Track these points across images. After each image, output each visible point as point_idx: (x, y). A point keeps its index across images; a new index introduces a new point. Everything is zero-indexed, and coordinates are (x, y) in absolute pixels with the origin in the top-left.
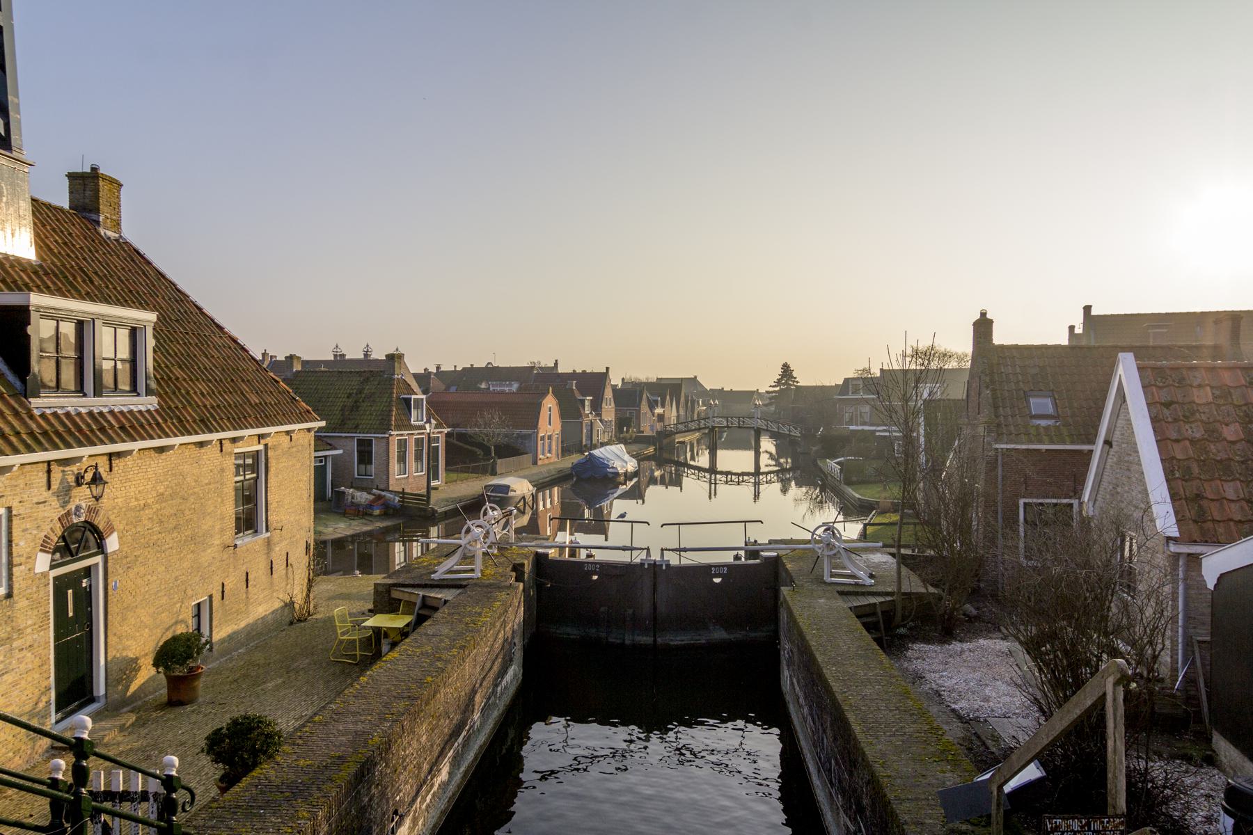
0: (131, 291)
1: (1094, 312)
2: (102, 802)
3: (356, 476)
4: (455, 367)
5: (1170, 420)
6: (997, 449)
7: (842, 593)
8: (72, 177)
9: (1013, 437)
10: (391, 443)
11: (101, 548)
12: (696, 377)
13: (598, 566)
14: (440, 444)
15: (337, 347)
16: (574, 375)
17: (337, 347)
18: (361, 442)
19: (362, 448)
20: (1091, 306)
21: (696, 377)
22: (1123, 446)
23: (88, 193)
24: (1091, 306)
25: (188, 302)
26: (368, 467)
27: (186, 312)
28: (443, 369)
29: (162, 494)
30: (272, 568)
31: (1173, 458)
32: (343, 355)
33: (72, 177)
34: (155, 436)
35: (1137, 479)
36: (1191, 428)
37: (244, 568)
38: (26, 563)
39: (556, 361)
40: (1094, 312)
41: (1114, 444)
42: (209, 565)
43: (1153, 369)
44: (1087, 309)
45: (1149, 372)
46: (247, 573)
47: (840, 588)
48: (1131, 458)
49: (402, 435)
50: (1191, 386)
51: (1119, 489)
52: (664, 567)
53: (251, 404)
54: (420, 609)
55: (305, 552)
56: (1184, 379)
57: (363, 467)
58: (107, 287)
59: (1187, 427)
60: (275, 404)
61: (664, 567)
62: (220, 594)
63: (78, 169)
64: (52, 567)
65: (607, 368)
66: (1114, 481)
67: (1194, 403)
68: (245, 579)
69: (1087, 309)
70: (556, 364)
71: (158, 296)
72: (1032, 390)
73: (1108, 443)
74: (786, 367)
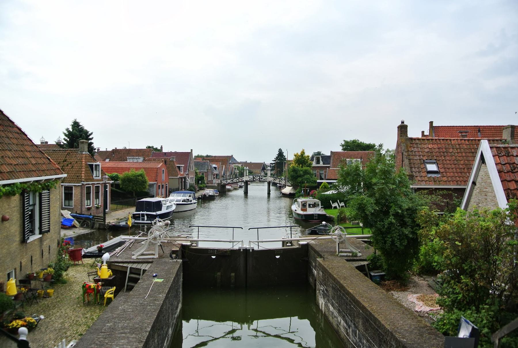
1: (434, 125)
4: (106, 149)
5: (505, 171)
7: (347, 260)
10: (83, 188)
12: (232, 156)
13: (216, 251)
15: (43, 137)
16: (171, 154)
17: (43, 137)
18: (66, 188)
19: (67, 192)
20: (433, 122)
21: (232, 156)
22: (482, 184)
24: (433, 122)
28: (101, 150)
30: (42, 254)
31: (509, 189)
32: (47, 142)
34: (20, 177)
35: (491, 200)
36: (515, 175)
37: (30, 253)
39: (162, 146)
40: (434, 125)
41: (477, 183)
42: (14, 252)
43: (497, 148)
44: (431, 123)
45: (495, 149)
46: (32, 257)
47: (346, 258)
48: (487, 190)
49: (89, 184)
50: (513, 156)
51: (480, 205)
52: (251, 251)
54: (129, 274)
55: (57, 245)
56: (509, 152)
57: (67, 202)
59: (513, 174)
61: (251, 251)
62: (20, 267)
65: (192, 150)
66: (477, 201)
67: (515, 164)
68: (30, 260)
69: (431, 123)
70: (162, 147)
72: (427, 160)
73: (474, 183)
74: (280, 150)
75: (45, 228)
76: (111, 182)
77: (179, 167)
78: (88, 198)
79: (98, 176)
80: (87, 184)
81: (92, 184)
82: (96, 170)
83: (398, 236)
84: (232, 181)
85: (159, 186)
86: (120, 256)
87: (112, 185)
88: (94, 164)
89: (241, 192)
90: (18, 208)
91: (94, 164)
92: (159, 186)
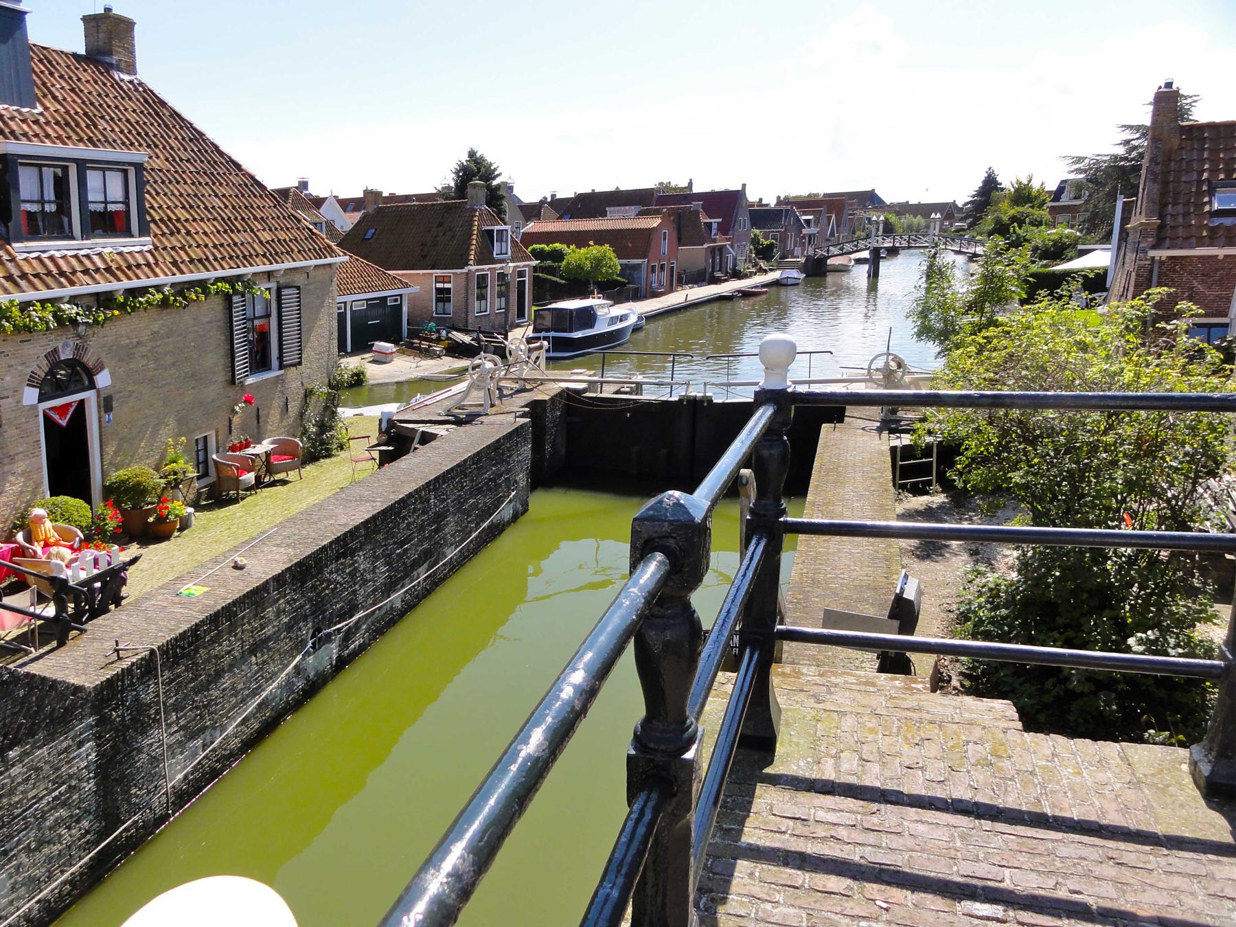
0: (139, 134)
2: (697, 906)
3: (434, 315)
6: (1153, 258)
8: (87, 20)
9: (1179, 241)
11: (92, 386)
14: (526, 279)
23: (101, 35)
25: (203, 140)
26: (447, 304)
27: (199, 151)
29: (156, 333)
33: (87, 20)
38: (13, 396)
42: (213, 401)
49: (482, 270)
53: (261, 242)
57: (440, 305)
58: (113, 131)
60: (291, 240)
63: (91, 12)
64: (40, 400)
70: (690, 183)
71: (170, 137)
75: (288, 360)
76: (535, 263)
77: (709, 225)
78: (482, 297)
79: (504, 251)
80: (477, 270)
81: (489, 269)
82: (500, 240)
83: (84, 656)
84: (856, 246)
85: (653, 267)
86: (110, 450)
87: (535, 269)
88: (496, 228)
89: (860, 275)
90: (221, 323)
91: (496, 228)
92: (653, 267)
